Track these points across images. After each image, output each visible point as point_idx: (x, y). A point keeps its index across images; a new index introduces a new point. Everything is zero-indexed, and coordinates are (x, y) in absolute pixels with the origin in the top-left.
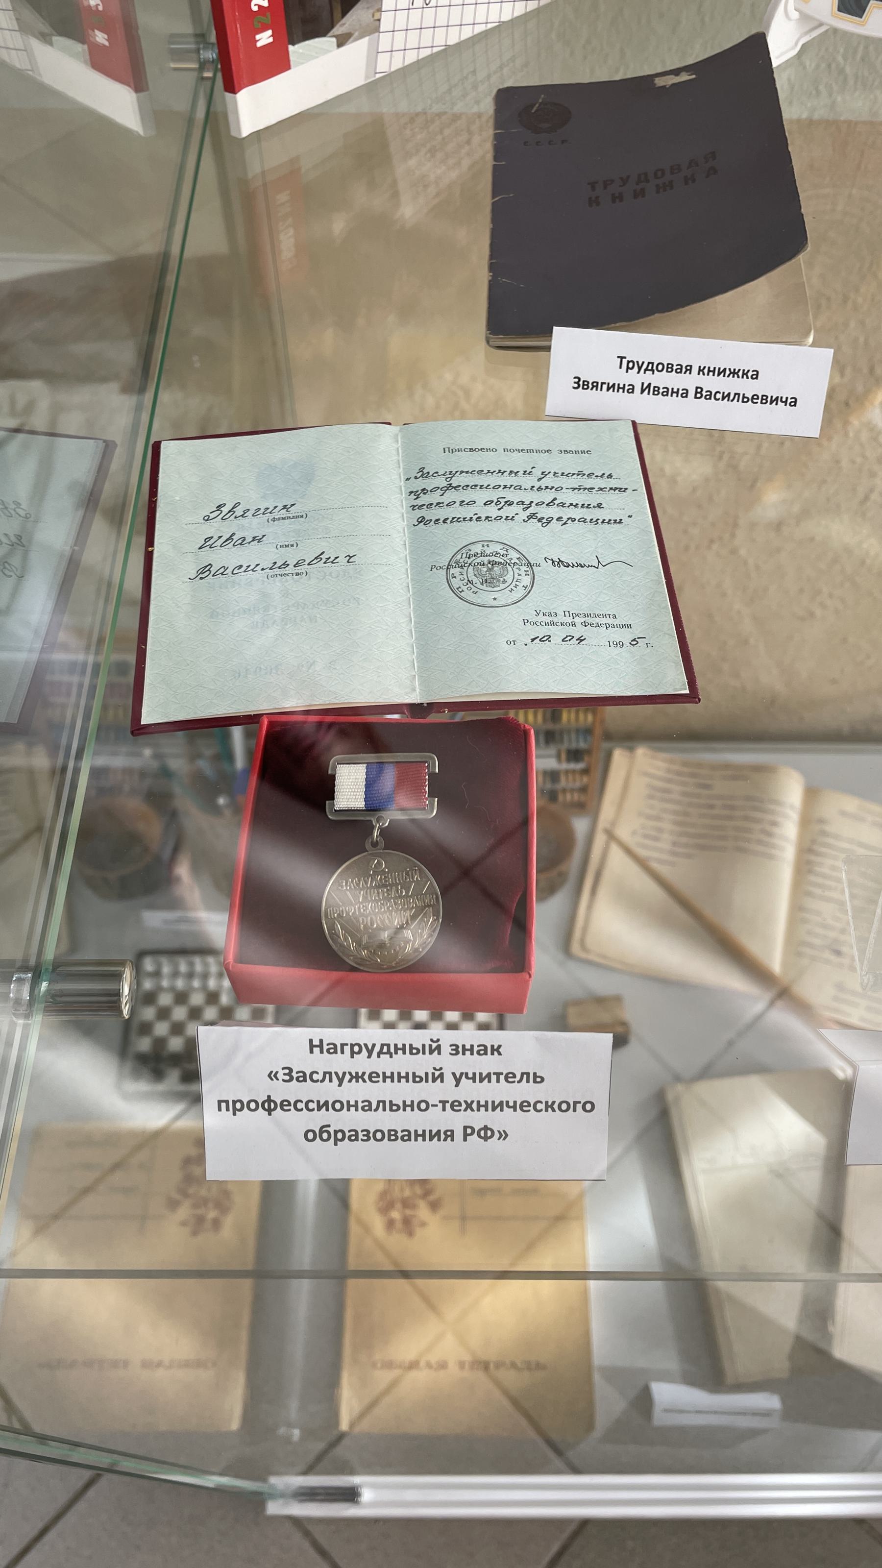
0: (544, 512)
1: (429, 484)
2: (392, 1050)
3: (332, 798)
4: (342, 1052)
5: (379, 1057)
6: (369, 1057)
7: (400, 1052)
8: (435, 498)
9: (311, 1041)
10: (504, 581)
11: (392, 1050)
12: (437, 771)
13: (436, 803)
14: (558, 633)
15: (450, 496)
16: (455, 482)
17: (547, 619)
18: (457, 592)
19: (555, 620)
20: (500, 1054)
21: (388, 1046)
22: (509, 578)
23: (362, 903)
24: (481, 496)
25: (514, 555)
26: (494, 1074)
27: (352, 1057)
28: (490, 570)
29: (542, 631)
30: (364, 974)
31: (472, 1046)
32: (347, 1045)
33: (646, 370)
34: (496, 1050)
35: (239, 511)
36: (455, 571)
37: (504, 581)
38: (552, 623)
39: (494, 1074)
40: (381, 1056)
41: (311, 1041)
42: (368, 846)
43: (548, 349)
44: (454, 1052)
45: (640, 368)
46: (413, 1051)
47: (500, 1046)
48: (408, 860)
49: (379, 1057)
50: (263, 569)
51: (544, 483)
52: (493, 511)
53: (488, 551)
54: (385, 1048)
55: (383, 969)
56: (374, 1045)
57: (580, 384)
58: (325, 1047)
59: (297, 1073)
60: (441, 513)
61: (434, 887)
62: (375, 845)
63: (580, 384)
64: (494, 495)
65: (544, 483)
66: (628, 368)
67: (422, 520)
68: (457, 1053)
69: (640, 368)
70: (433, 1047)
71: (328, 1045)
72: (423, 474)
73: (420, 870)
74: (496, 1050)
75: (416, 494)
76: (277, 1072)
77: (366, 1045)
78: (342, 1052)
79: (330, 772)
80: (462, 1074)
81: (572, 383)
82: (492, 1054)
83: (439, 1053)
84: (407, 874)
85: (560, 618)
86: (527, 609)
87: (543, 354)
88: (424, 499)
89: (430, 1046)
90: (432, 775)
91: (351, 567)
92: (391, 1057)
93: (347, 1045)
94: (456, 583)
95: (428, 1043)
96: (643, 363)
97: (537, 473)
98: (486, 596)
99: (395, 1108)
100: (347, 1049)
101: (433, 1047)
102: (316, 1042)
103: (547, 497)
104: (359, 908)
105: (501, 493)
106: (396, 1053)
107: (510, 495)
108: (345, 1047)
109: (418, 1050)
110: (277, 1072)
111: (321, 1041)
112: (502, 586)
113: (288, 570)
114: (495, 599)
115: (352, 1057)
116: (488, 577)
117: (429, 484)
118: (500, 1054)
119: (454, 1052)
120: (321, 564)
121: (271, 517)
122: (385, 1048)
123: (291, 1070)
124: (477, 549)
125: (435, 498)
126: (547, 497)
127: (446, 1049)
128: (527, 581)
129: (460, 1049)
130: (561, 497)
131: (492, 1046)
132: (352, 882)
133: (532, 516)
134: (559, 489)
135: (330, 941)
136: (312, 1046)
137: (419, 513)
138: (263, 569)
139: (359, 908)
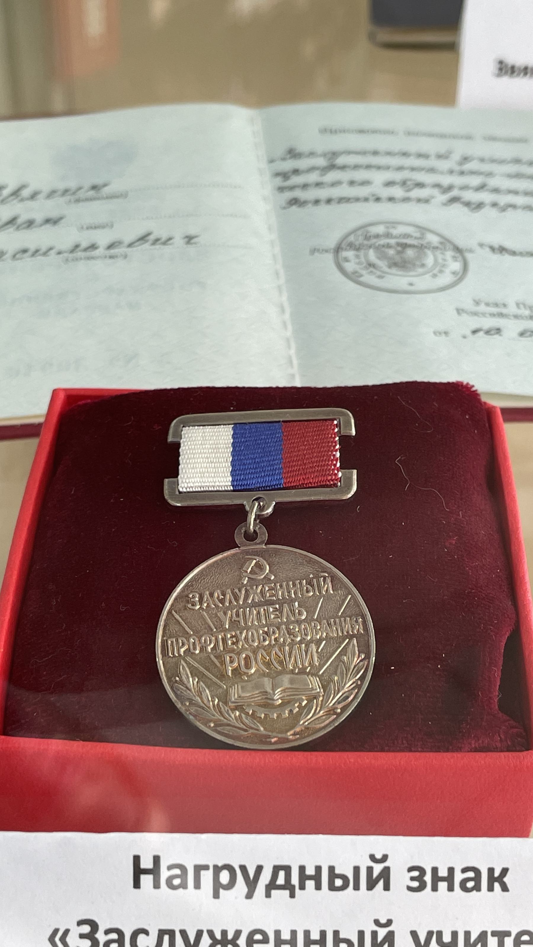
0: (469, 196)
1: (302, 164)
2: (295, 880)
3: (175, 473)
4: (197, 885)
5: (268, 895)
6: (249, 896)
7: (310, 884)
8: (313, 177)
9: (137, 859)
10: (423, 265)
11: (295, 880)
12: (354, 433)
13: (355, 477)
14: (512, 328)
15: (332, 176)
16: (340, 161)
17: (494, 310)
18: (354, 277)
19: (504, 311)
20: (505, 888)
21: (287, 869)
22: (430, 260)
23: (229, 630)
24: (379, 178)
25: (434, 239)
26: (494, 934)
27: (216, 895)
28: (399, 253)
29: (488, 323)
30: (235, 753)
31: (451, 870)
32: (206, 868)
33: (272, 886)
34: (498, 879)
35: (25, 193)
36: (350, 254)
37: (423, 265)
38: (501, 315)
39: (494, 934)
40: (273, 892)
41: (137, 859)
42: (239, 539)
43: (452, 48)
44: (415, 884)
45: (252, 885)
46: (338, 882)
47: (505, 871)
48: (310, 561)
49: (268, 895)
50: (59, 253)
51: (467, 167)
52: (398, 192)
53: (395, 232)
54: (282, 874)
55: (271, 743)
56: (259, 869)
57: (505, 69)
58: (165, 874)
59: (107, 932)
60: (323, 193)
61: (358, 605)
62: (251, 537)
63: (505, 69)
64: (398, 176)
65: (467, 167)
66: (217, 887)
67: (294, 202)
68: (422, 887)
69: (252, 885)
70: (375, 874)
71: (170, 868)
72: (293, 154)
73: (333, 578)
74: (498, 879)
75: (285, 176)
76: (67, 932)
77: (243, 868)
78: (197, 885)
79: (170, 439)
80: (430, 934)
81: (492, 67)
82: (491, 889)
83: (387, 888)
84: (310, 583)
85: (512, 309)
86: (465, 294)
87: (444, 56)
88: (296, 180)
89: (370, 870)
90: (345, 440)
91: (191, 250)
92: (292, 895)
93: (206, 868)
94: (349, 267)
95: (365, 863)
96: (259, 869)
97: (456, 157)
98: (399, 280)
99: (338, 882)
100: (207, 877)
101: (375, 874)
102: (146, 863)
103: (476, 181)
104: (224, 640)
105: (405, 174)
106: (302, 887)
107: (420, 177)
108: (203, 873)
109: (344, 878)
110: (67, 932)
111: (157, 860)
112: (420, 270)
113: (96, 253)
114: (411, 284)
115: (216, 895)
116: (397, 259)
117: (302, 164)
118: (505, 888)
119: (415, 884)
120: (147, 246)
121: (73, 198)
122: (282, 874)
123: (94, 925)
124: (380, 229)
125: (313, 177)
126: (476, 181)
127: (401, 878)
128: (457, 266)
129: (428, 878)
130: (493, 182)
131: (491, 871)
132: (211, 595)
133: (455, 200)
134: (490, 174)
135: (172, 695)
136: (138, 872)
137: (289, 195)
138: (59, 253)
139: (224, 640)
